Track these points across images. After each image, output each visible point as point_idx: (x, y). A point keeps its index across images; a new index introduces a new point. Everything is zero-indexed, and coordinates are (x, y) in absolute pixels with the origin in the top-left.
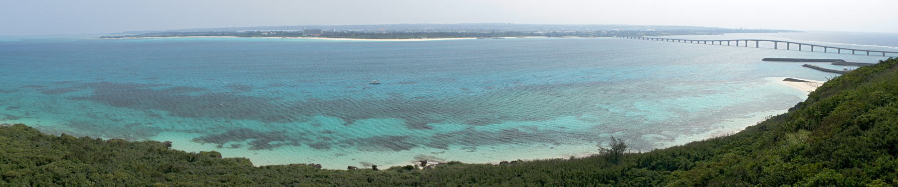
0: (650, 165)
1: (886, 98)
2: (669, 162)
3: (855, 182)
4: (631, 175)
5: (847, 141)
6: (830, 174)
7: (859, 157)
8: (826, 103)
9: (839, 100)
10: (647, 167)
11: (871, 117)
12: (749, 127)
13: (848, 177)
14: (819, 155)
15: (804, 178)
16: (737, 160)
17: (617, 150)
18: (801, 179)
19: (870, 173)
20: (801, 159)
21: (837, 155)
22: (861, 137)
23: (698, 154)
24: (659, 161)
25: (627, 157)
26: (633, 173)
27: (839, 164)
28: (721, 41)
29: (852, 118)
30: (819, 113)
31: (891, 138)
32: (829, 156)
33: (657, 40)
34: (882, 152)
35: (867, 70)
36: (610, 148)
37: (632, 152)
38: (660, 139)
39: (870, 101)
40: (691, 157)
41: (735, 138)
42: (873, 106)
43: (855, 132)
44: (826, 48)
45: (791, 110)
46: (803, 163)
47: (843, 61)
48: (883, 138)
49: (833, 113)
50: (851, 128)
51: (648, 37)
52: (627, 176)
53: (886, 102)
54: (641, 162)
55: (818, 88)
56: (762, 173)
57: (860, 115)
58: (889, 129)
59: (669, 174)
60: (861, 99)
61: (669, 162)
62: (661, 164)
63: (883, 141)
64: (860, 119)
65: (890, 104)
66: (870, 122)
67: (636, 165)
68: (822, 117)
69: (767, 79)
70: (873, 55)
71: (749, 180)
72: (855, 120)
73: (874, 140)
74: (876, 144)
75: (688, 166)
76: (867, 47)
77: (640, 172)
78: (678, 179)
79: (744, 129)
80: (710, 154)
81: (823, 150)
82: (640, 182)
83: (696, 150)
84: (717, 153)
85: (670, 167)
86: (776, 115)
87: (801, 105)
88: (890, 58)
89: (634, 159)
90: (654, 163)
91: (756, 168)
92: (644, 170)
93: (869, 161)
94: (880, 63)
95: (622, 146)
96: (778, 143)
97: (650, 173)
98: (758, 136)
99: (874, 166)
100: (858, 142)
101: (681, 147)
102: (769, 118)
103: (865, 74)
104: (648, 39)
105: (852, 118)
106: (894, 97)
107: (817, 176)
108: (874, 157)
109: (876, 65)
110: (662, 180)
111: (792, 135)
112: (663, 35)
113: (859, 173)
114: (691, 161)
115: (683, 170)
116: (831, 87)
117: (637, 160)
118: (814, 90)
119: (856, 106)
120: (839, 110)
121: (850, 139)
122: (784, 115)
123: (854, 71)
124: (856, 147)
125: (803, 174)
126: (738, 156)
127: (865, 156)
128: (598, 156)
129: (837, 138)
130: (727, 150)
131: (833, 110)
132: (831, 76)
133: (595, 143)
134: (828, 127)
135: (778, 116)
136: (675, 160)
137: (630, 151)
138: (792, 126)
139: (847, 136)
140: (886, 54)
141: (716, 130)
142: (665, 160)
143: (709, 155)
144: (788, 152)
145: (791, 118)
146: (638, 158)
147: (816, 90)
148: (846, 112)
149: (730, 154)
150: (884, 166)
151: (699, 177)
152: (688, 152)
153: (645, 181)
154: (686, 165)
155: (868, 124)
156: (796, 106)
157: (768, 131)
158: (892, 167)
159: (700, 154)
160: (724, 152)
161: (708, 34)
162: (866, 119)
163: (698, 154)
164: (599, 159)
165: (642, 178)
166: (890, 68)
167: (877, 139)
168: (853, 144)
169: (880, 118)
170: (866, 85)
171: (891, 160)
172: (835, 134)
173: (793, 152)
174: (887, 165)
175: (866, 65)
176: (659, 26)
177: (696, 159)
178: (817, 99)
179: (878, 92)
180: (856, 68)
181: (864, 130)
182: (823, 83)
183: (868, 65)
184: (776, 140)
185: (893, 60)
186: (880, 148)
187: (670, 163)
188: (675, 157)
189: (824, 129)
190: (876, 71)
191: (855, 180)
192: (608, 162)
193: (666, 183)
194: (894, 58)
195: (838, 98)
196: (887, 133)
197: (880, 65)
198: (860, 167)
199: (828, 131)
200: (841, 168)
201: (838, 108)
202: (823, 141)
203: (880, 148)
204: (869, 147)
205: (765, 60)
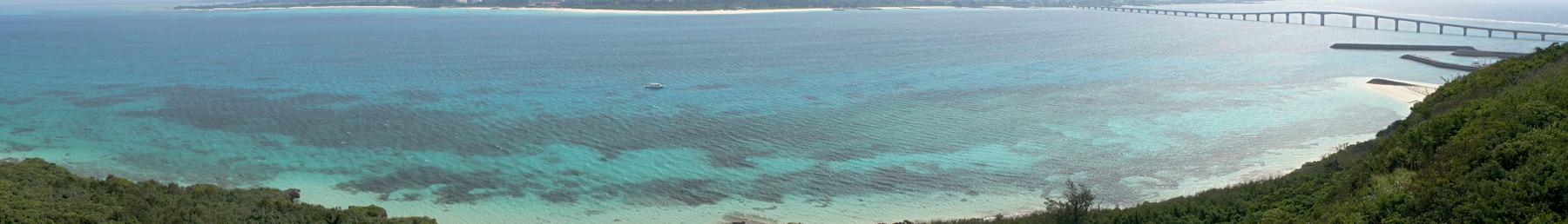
7: (1500, 215)
9: (1465, 117)
12: (1308, 164)
21: (1461, 213)
22: (1503, 181)
23: (1219, 212)
25: (1095, 216)
28: (1258, 15)
29: (1488, 149)
31: (1555, 183)
34: (1541, 208)
35: (1514, 65)
36: (1064, 201)
37: (1103, 207)
38: (1152, 185)
39: (1520, 119)
41: (1284, 182)
44: (1441, 26)
45: (1380, 134)
47: (1472, 48)
48: (1542, 183)
49: (1455, 140)
50: (1486, 166)
51: (1131, 7)
57: (1502, 143)
65: (1554, 125)
66: (1519, 155)
68: (1435, 146)
70: (1526, 39)
72: (1494, 151)
74: (1529, 193)
76: (1513, 24)
79: (1299, 167)
81: (1437, 204)
87: (1399, 126)
88: (1553, 44)
94: (1537, 53)
95: (1086, 197)
96: (1357, 191)
98: (1323, 180)
100: (1498, 190)
101: (1190, 198)
102: (1343, 149)
103: (1510, 72)
105: (1488, 149)
106: (1561, 112)
108: (1526, 216)
109: (1529, 56)
116: (1450, 94)
118: (1421, 99)
120: (1466, 134)
121: (1484, 184)
123: (1491, 66)
124: (1494, 198)
129: (1461, 182)
131: (1454, 134)
132: (1451, 76)
133: (1040, 192)
135: (1359, 145)
137: (1101, 205)
138: (1382, 162)
139: (1480, 179)
140: (1546, 37)
141: (1251, 169)
143: (1238, 212)
144: (1376, 207)
147: (1425, 100)
148: (1478, 137)
149: (1275, 211)
152: (1202, 207)
155: (1516, 158)
157: (1341, 170)
159: (1222, 210)
163: (1219, 212)
166: (1555, 61)
167: (1532, 184)
168: (1489, 193)
169: (1536, 147)
170: (1512, 90)
172: (1457, 176)
173: (1384, 207)
175: (1511, 56)
178: (1426, 116)
180: (1494, 61)
181: (1508, 169)
182: (1437, 87)
183: (1515, 56)
184: (1354, 186)
185: (1559, 47)
186: (1536, 200)
188: (1179, 217)
189: (1439, 168)
190: (1530, 67)
195: (1464, 114)
196: (1550, 175)
201: (1463, 131)
202: (1436, 189)
203: (1536, 200)
204: (1518, 198)
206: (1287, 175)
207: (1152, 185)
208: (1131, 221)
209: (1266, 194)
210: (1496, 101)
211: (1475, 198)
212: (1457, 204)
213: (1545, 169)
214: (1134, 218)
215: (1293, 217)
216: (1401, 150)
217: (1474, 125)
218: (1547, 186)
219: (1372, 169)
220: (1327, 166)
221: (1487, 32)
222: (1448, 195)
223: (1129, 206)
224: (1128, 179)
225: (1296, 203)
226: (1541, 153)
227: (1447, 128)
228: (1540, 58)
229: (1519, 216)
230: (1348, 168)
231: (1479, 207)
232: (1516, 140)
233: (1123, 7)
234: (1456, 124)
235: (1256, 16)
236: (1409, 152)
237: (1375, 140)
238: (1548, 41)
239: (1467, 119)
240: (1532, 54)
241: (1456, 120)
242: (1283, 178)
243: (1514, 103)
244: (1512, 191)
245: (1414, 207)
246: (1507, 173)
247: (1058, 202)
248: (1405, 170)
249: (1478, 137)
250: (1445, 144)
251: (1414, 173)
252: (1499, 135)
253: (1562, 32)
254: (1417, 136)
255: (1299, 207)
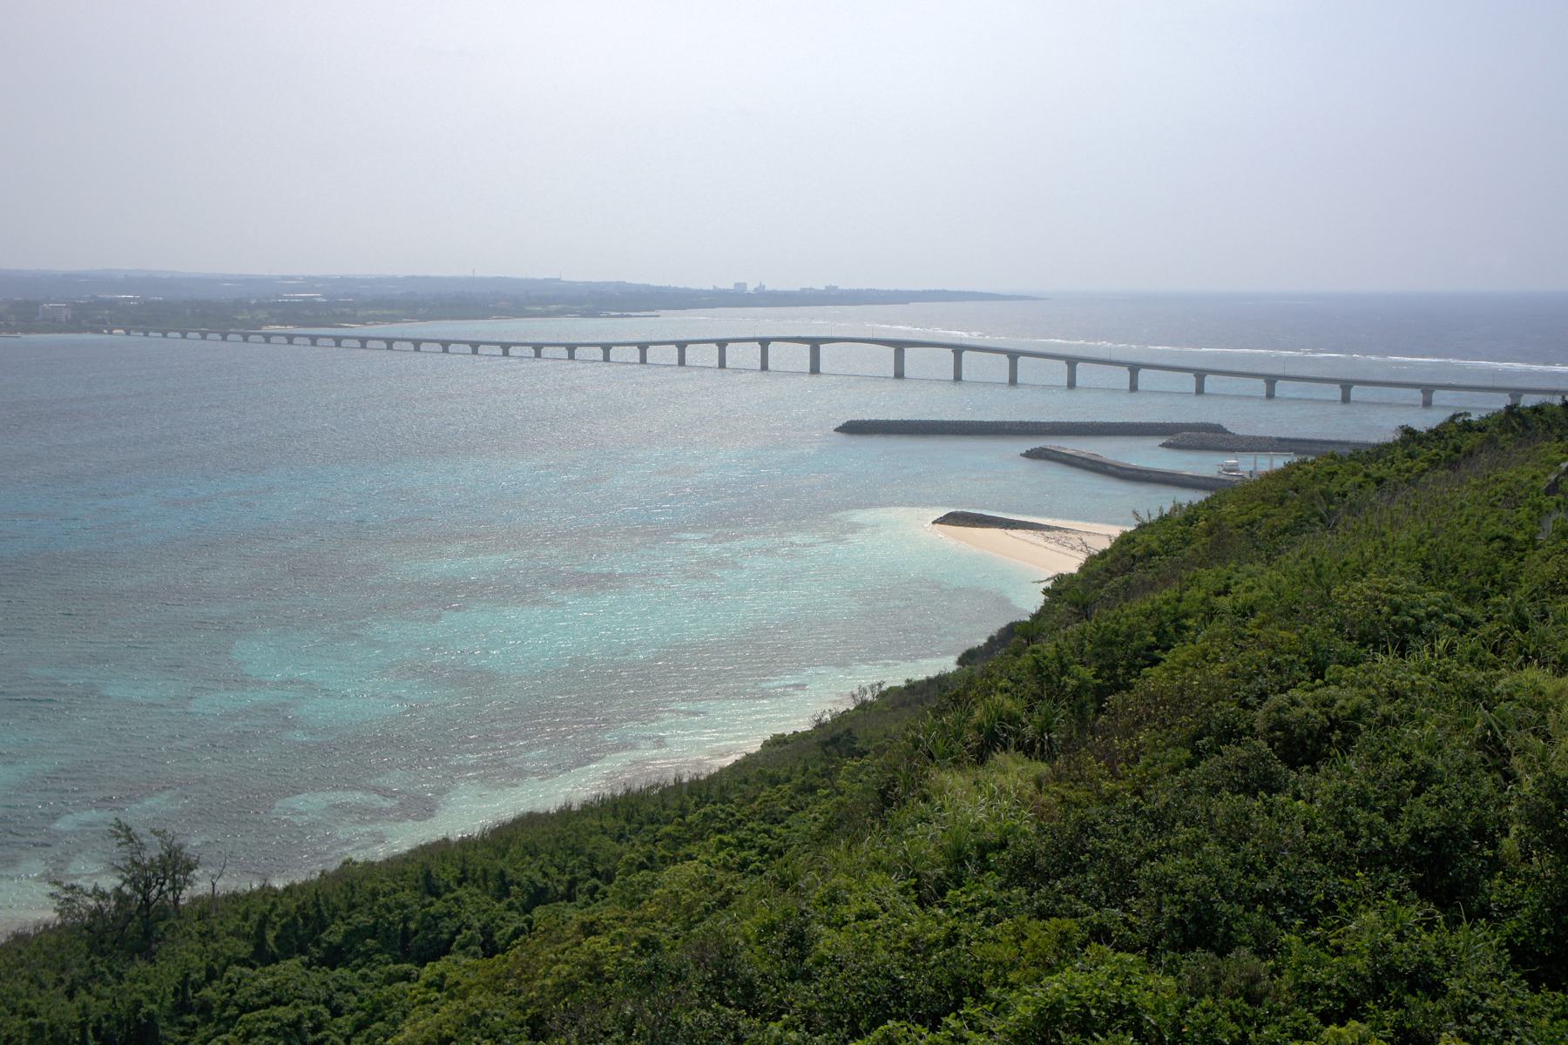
0: (317, 944)
1: (1422, 613)
2: (406, 920)
3: (1233, 1027)
4: (225, 1005)
5: (1210, 817)
6: (1112, 976)
7: (1265, 898)
8: (1124, 628)
9: (1186, 616)
10: (303, 951)
11: (1340, 703)
12: (778, 741)
13: (1201, 996)
14: (1071, 880)
15: (994, 992)
16: (718, 895)
17: (148, 886)
18: (978, 993)
19: (1314, 987)
20: (994, 894)
21: (1156, 883)
22: (1280, 798)
23: (545, 875)
24: (362, 919)
25: (202, 916)
26: (232, 992)
27: (1162, 926)
28: (682, 346)
29: (1244, 705)
30: (1087, 673)
31: (1432, 818)
32: (1121, 886)
33: (290, 342)
34: (1386, 884)
35: (1332, 474)
36: (109, 883)
37: (226, 885)
38: (364, 813)
39: (1340, 628)
40: (514, 889)
41: (715, 791)
42: (1349, 648)
43: (1252, 774)
44: (1134, 369)
45: (968, 658)
46: (996, 913)
47: (1218, 429)
48: (1391, 815)
49: (1154, 678)
50: (1234, 753)
51: (290, 329)
52: (205, 1008)
53: (1418, 632)
54: (270, 936)
55: (1092, 559)
56: (808, 961)
57: (1283, 690)
58: (1429, 769)
59: (406, 977)
60: (1290, 612)
61: (406, 920)
62: (373, 932)
63: (1389, 829)
64: (1280, 710)
65: (1440, 645)
66: (1331, 729)
67: (245, 949)
68: (1101, 694)
69: (859, 516)
70: (1389, 405)
71: (749, 1000)
72: (1260, 713)
73: (1342, 821)
74: (1352, 837)
75: (497, 935)
76: (1328, 359)
77: (266, 982)
78: (452, 997)
79: (754, 747)
80: (600, 869)
81: (1096, 855)
82: (269, 1032)
83: (534, 854)
84: (630, 863)
85: (415, 942)
86: (903, 684)
87: (1017, 636)
88: (1455, 416)
89: (234, 922)
90: (335, 934)
91: (782, 936)
92: (290, 969)
93: (1313, 922)
94: (1403, 443)
95: (176, 865)
96: (897, 815)
97: (318, 981)
98: (818, 782)
99: (1338, 951)
100: (1261, 822)
101: (465, 843)
102: (869, 697)
103: (1322, 493)
104: (290, 339)
105: (1244, 705)
106: (1466, 610)
107: (1055, 985)
108: (1341, 907)
109: (1379, 452)
110: (376, 1013)
111: (959, 779)
112: (363, 321)
113: (1255, 980)
114: (510, 907)
115: (475, 955)
116: (1151, 554)
117: (250, 927)
118: (1071, 564)
119: (1264, 646)
120: (1185, 664)
121: (1224, 805)
122: (938, 683)
123: (1268, 476)
124: (1248, 847)
125: (987, 974)
126: (720, 876)
127: (1290, 892)
128: (47, 929)
129: (1161, 798)
130: (677, 846)
131: (1155, 662)
132: (1157, 502)
133: (36, 866)
134: (1126, 745)
135: (912, 687)
136: (439, 906)
137: (220, 884)
138: (958, 736)
139: (1214, 790)
140: (1438, 397)
141: (626, 757)
142: (390, 911)
143: (595, 874)
144: (940, 858)
145: (956, 700)
146: (255, 917)
147: (1081, 569)
148: (1219, 669)
149: (689, 869)
150: (1386, 959)
151: (549, 982)
152: (500, 864)
153: (296, 1024)
154: (487, 931)
155: (1323, 735)
156: (991, 639)
157: (862, 754)
158: (1428, 966)
159: (553, 871)
160: (663, 857)
161: (583, 316)
162: (1314, 712)
163: (545, 875)
164: (59, 947)
165: (278, 1011)
166: (1452, 465)
167: (1361, 815)
168: (1235, 834)
169: (1384, 709)
170: (1320, 545)
171: (1429, 928)
172: (1155, 778)
173: (958, 858)
174: (1405, 955)
175: (1330, 450)
176: (344, 281)
177: (539, 896)
178: (1083, 610)
179: (1382, 582)
180: (1279, 462)
181: (1293, 765)
182: (1116, 531)
183: (1338, 451)
184: (886, 799)
185: (1468, 427)
186: (1371, 860)
187: (412, 926)
188: (438, 896)
189: (1109, 756)
190: (1380, 481)
191: (1234, 1019)
192: (102, 953)
193: (395, 1022)
194: (1474, 417)
195: (1183, 607)
196: (1417, 792)
197: (1399, 452)
198: (1263, 952)
199: (1128, 761)
200: (1174, 946)
201: (1179, 653)
202: (1095, 811)
203: (1371, 860)
204: (1319, 853)
205: (854, 429)
206: (722, 770)
207: (364, 813)
208: (306, 918)
209: (668, 821)
210: (1272, 574)
211: (1198, 843)
212: (1151, 856)
213: (1408, 775)
214: (312, 912)
215: (734, 882)
216: (1008, 703)
217: (1211, 638)
218: (1405, 822)
219: (931, 756)
220: (827, 744)
221: (1190, 380)
222: (1126, 831)
223: (299, 878)
224: (299, 802)
225: (741, 844)
226: (1395, 724)
227: (1136, 643)
228: (1411, 456)
229: (1319, 904)
230: (880, 751)
231: (1208, 871)
232: (1327, 684)
233: (265, 329)
234: (1160, 633)
235: (674, 350)
236: (1031, 710)
237: (954, 674)
238: (1443, 407)
239: (1190, 622)
240: (1388, 446)
241: (1161, 624)
242: (712, 779)
243: (1325, 580)
244: (1300, 832)
245: (1033, 859)
246: (1293, 775)
247: (89, 887)
248: (1020, 755)
249: (1219, 669)
250: (1129, 687)
251: (1042, 768)
252: (1277, 668)
253: (1490, 384)
254: (1055, 666)
255: (752, 854)
